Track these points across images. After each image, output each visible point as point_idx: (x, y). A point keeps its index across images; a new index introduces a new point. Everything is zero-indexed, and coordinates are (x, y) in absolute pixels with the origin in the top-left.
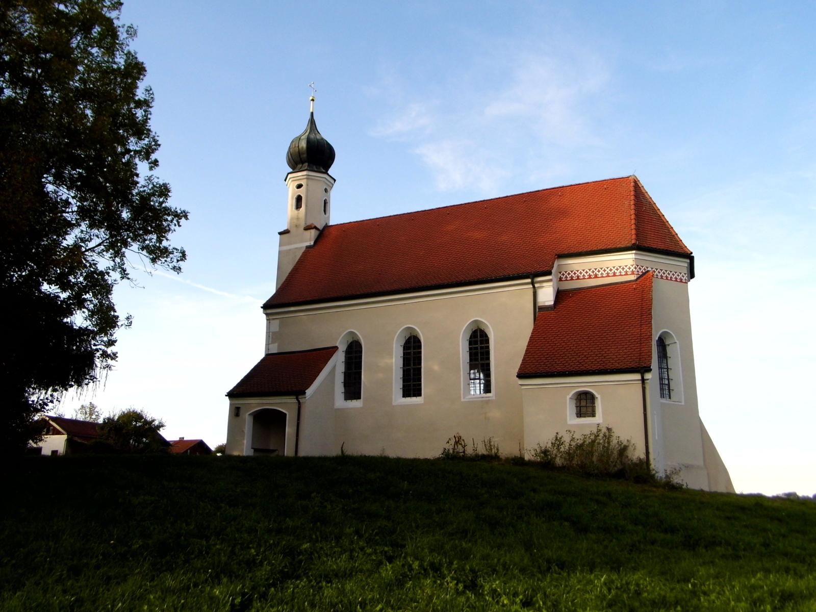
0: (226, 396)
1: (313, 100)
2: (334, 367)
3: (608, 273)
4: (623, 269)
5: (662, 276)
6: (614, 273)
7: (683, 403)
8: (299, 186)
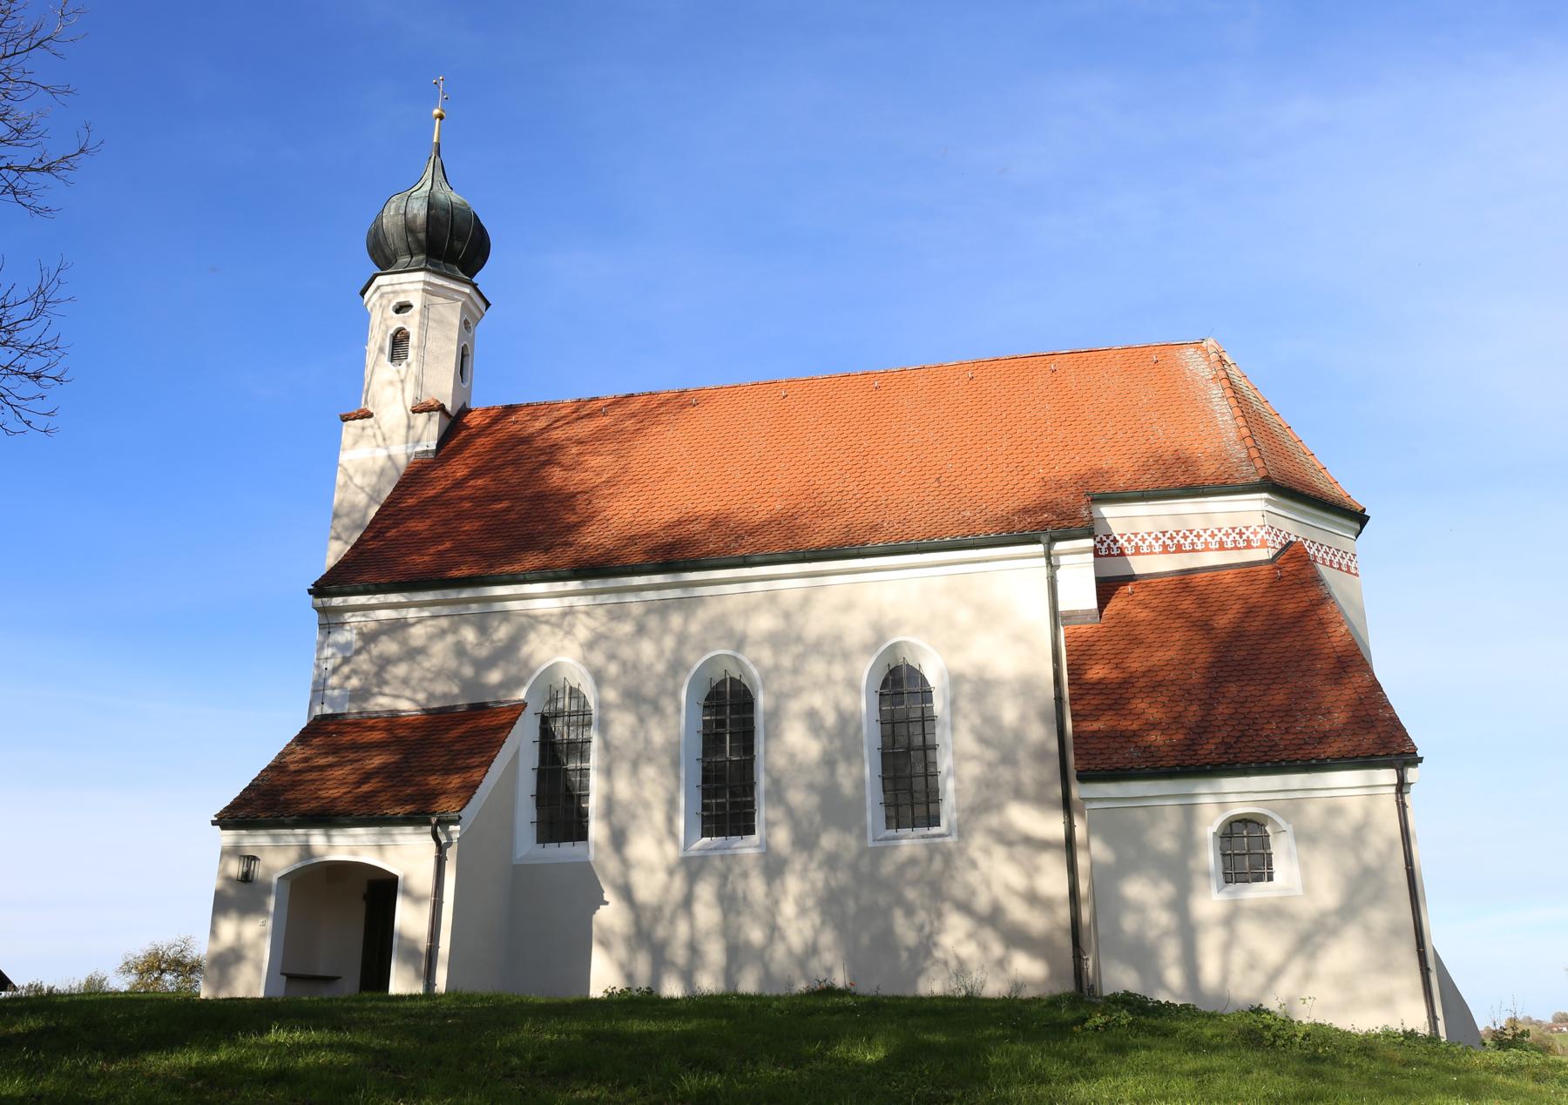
0: (214, 823)
1: (441, 117)
2: (516, 754)
3: (1206, 543)
4: (1241, 534)
5: (1165, 546)
6: (1221, 543)
8: (402, 308)
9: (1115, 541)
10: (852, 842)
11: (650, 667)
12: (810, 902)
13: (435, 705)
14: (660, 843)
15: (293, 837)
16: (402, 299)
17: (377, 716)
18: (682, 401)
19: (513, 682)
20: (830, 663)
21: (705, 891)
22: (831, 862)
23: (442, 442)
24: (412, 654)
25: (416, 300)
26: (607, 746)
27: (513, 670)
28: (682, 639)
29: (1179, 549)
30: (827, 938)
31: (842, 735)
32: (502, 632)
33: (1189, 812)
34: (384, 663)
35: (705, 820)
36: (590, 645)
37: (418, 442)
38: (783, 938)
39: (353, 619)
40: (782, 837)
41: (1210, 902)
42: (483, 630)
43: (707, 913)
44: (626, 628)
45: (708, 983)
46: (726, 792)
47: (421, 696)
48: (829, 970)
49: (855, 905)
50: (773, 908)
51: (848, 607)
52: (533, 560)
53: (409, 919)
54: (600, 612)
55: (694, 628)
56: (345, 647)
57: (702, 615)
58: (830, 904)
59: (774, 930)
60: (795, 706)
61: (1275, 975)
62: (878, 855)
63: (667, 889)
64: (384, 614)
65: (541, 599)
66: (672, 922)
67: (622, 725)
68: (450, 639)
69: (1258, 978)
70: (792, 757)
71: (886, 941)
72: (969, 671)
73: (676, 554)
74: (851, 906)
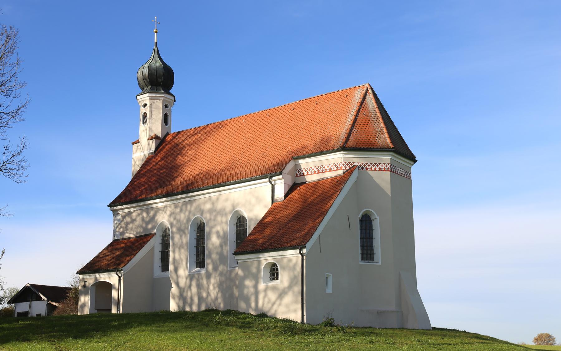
1: (156, 32)
7: (380, 264)
9: (302, 171)
10: (226, 268)
11: (183, 221)
12: (216, 285)
13: (138, 235)
14: (184, 270)
15: (93, 276)
16: (144, 103)
17: (125, 239)
18: (219, 126)
19: (153, 228)
20: (222, 217)
21: (194, 283)
22: (221, 274)
23: (156, 150)
24: (133, 221)
25: (148, 102)
26: (173, 244)
27: (153, 224)
28: (190, 212)
29: (319, 172)
30: (220, 295)
31: (224, 238)
32: (152, 213)
33: (259, 261)
34: (127, 224)
35: (197, 263)
36: (170, 215)
37: (150, 149)
38: (210, 295)
39: (120, 212)
40: (210, 267)
41: (262, 286)
42: (148, 213)
43: (194, 289)
44: (178, 210)
45: (195, 308)
46: (200, 257)
47: (135, 233)
48: (220, 304)
49: (228, 285)
50: (208, 288)
51: (227, 200)
52: (160, 191)
53: (115, 294)
54: (172, 206)
55: (193, 209)
56: (119, 220)
57: (195, 205)
58: (220, 285)
59: (208, 294)
60: (214, 230)
61: (274, 304)
62: (231, 272)
63: (186, 283)
64: (126, 210)
65: (159, 203)
66: (187, 292)
67: (177, 238)
68: (141, 216)
69: (270, 305)
70: (213, 244)
71: (232, 295)
72: (254, 217)
73: (190, 187)
74: (225, 286)
